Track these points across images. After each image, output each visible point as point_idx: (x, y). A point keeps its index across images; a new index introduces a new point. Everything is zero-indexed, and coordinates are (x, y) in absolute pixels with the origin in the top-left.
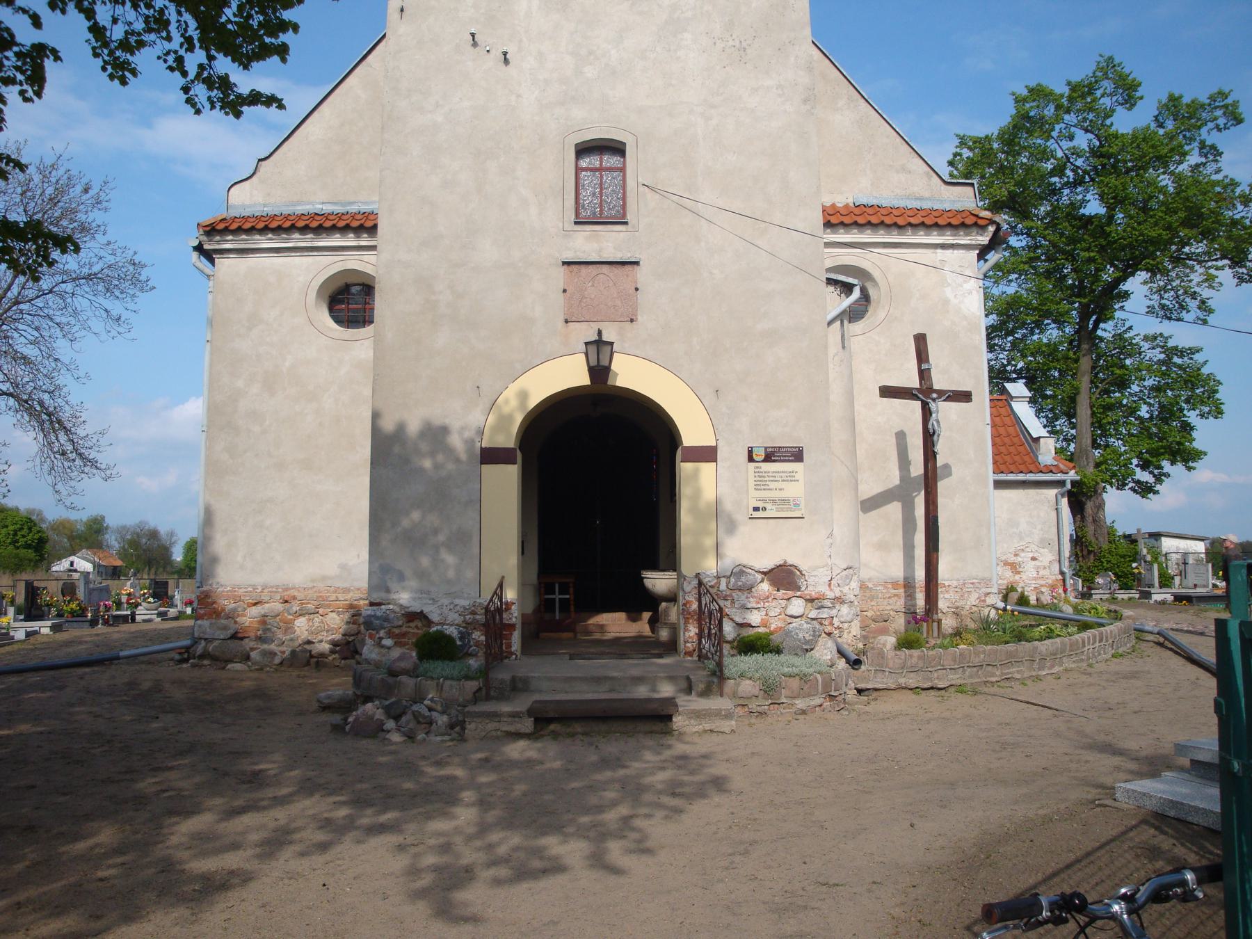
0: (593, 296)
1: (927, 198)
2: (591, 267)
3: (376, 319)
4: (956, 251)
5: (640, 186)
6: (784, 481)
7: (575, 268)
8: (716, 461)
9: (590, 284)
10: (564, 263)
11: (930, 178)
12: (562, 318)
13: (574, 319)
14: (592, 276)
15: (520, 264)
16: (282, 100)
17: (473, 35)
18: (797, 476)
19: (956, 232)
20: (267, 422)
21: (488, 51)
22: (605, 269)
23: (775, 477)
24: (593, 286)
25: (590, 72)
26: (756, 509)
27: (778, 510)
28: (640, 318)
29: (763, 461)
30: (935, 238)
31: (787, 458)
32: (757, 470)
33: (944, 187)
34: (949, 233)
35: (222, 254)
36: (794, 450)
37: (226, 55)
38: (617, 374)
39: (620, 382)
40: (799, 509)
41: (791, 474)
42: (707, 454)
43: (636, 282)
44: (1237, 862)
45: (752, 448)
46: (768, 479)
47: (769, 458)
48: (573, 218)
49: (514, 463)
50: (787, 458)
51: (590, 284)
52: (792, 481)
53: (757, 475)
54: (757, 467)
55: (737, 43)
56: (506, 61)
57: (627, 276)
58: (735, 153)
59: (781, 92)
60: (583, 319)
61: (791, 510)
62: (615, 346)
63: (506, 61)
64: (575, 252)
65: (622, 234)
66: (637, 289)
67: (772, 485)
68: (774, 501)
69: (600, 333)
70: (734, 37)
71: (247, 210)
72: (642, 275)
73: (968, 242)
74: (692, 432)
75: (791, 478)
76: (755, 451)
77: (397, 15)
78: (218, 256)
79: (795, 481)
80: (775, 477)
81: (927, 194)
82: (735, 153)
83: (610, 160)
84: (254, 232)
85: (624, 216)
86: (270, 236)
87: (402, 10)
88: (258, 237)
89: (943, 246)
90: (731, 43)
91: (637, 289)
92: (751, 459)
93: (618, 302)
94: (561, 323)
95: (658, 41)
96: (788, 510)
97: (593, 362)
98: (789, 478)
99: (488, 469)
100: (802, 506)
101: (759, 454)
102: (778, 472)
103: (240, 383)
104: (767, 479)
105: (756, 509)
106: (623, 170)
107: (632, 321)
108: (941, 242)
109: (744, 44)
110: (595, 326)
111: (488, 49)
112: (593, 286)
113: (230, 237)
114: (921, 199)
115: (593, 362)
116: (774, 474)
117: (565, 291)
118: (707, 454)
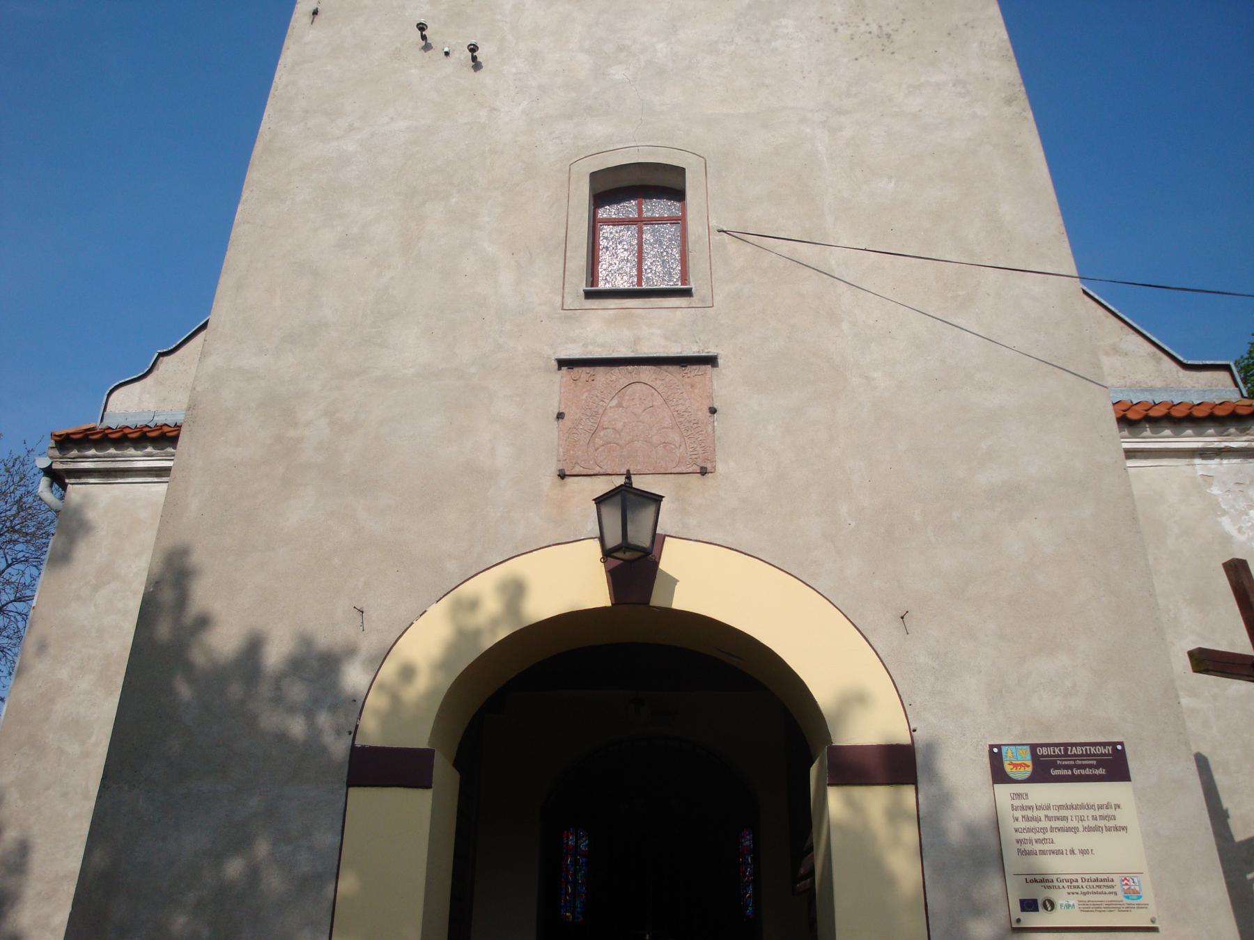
0: (619, 425)
1: (1160, 389)
2: (616, 370)
4: (1225, 461)
5: (714, 232)
6: (1089, 829)
7: (583, 372)
9: (614, 402)
10: (563, 363)
11: (1159, 361)
13: (577, 470)
14: (619, 387)
15: (473, 370)
17: (422, 27)
18: (1122, 818)
19: (1222, 429)
20: (93, 739)
21: (447, 54)
22: (646, 373)
23: (1064, 818)
24: (619, 405)
25: (618, 73)
27: (1086, 908)
28: (720, 467)
29: (1030, 780)
30: (1189, 440)
31: (1088, 772)
32: (1017, 803)
33: (1183, 374)
34: (1211, 431)
35: (79, 478)
36: (1102, 750)
38: (675, 581)
39: (683, 601)
40: (1140, 907)
41: (1104, 812)
43: (711, 397)
45: (999, 746)
46: (1047, 824)
48: (583, 287)
49: (425, 784)
50: (1088, 772)
51: (614, 402)
52: (1109, 829)
53: (1019, 814)
54: (1019, 796)
56: (477, 65)
57: (692, 386)
58: (890, 177)
59: (963, 90)
60: (597, 470)
62: (664, 504)
63: (477, 65)
64: (585, 345)
65: (679, 313)
66: (713, 411)
70: (867, 20)
71: (129, 419)
73: (1245, 444)
75: (1105, 821)
76: (1008, 754)
77: (306, 20)
78: (73, 481)
79: (1116, 829)
80: (1064, 818)
81: (1159, 384)
82: (890, 177)
83: (658, 208)
84: (127, 444)
85: (684, 277)
86: (150, 449)
87: (315, 13)
88: (132, 451)
89: (1204, 453)
90: (863, 28)
91: (713, 411)
93: (674, 437)
95: (738, 30)
96: (1111, 907)
98: (1101, 823)
99: (362, 798)
100: (1148, 895)
101: (1018, 761)
102: (1072, 807)
103: (64, 674)
104: (1044, 824)
106: (680, 221)
107: (704, 472)
108: (1200, 445)
109: (887, 30)
111: (446, 49)
112: (619, 405)
113: (92, 452)
114: (1151, 390)
116: (1063, 813)
117: (560, 416)
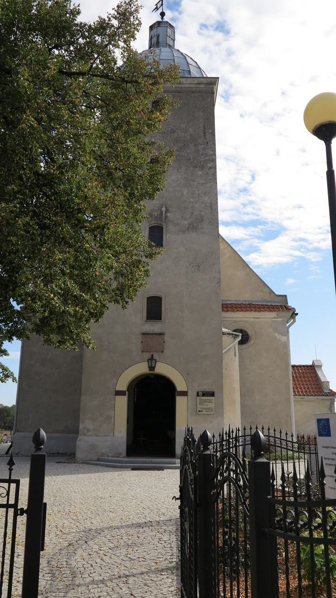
3: (146, 300)
7: (145, 335)
22: (155, 336)
28: (165, 351)
37: (2, 346)
42: (184, 394)
44: (198, 595)
47: (203, 395)
66: (164, 342)
67: (205, 404)
68: (205, 409)
69: (152, 356)
72: (166, 338)
74: (180, 386)
75: (210, 402)
81: (270, 299)
91: (164, 342)
92: (198, 395)
94: (140, 352)
97: (150, 365)
101: (201, 394)
107: (162, 352)
110: (151, 353)
114: (267, 302)
115: (150, 365)
117: (142, 342)
118: (184, 394)
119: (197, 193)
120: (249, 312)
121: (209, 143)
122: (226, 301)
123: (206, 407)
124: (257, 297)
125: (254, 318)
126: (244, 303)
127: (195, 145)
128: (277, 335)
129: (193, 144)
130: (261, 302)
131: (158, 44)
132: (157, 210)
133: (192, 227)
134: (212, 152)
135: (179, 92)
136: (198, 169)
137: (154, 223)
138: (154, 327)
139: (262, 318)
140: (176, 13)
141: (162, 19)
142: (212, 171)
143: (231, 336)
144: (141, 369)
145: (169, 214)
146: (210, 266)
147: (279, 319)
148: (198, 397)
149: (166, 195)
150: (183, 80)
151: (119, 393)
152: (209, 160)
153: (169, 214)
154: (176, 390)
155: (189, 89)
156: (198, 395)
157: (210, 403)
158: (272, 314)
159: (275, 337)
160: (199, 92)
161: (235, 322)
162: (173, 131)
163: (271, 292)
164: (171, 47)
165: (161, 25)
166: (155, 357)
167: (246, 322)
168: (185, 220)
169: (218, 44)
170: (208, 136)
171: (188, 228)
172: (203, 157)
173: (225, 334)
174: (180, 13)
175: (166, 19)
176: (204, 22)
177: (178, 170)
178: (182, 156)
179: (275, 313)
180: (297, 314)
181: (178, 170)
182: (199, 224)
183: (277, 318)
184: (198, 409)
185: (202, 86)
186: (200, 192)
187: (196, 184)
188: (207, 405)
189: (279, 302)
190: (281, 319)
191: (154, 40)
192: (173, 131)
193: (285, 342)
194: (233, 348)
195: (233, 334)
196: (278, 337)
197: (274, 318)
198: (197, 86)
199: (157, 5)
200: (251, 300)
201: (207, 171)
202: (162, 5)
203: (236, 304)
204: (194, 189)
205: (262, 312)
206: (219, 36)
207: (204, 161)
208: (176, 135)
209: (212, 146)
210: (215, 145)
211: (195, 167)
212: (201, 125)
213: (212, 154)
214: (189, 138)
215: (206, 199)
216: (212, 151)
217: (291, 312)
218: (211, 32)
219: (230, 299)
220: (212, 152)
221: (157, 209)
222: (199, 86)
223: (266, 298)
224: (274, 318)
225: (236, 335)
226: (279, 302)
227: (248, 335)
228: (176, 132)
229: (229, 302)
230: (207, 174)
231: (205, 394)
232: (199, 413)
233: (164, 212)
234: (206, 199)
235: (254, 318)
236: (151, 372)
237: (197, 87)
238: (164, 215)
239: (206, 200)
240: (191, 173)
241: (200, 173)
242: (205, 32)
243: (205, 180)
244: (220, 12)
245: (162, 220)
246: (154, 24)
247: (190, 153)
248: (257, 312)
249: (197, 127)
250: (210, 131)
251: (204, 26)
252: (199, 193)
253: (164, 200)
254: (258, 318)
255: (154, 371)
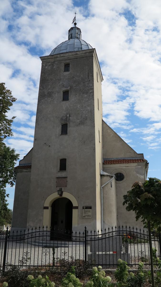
8: (44, 207)
12: (56, 186)
16: (15, 62)
18: (91, 211)
26: (84, 217)
27: (87, 217)
42: (77, 208)
55: (84, 141)
61: (89, 217)
67: (87, 213)
68: (87, 215)
72: (68, 179)
74: (75, 204)
75: (89, 211)
81: (134, 156)
92: (83, 209)
101: (84, 208)
105: (84, 217)
114: (133, 157)
117: (56, 182)
118: (77, 208)
119: (84, 106)
120: (122, 164)
121: (90, 81)
122: (111, 158)
123: (87, 214)
124: (128, 156)
125: (126, 167)
126: (121, 159)
127: (84, 83)
128: (138, 175)
129: (83, 82)
130: (130, 158)
131: (71, 38)
132: (65, 116)
133: (82, 123)
134: (92, 85)
135: (76, 59)
136: (85, 94)
137: (63, 122)
138: (63, 174)
139: (130, 166)
140: (134, 27)
141: (75, 26)
142: (92, 94)
143: (109, 177)
144: (55, 196)
145: (70, 118)
146: (90, 142)
147: (139, 167)
148: (83, 209)
149: (69, 108)
150: (78, 53)
151: (46, 208)
152: (90, 89)
153: (70, 118)
154: (73, 206)
155: (81, 57)
156: (83, 209)
157: (89, 212)
158: (135, 164)
159: (138, 176)
160: (86, 57)
161: (116, 169)
162: (73, 77)
163: (135, 152)
164: (78, 38)
165: (73, 29)
166: (63, 190)
167: (122, 169)
168: (78, 120)
169: (155, 37)
170: (90, 77)
171: (80, 123)
172: (87, 88)
173: (105, 176)
174: (136, 26)
175: (77, 26)
176: (147, 29)
177: (75, 95)
178: (77, 89)
179: (137, 163)
180: (148, 163)
181: (75, 95)
182: (85, 121)
183: (138, 166)
184: (83, 216)
185: (88, 54)
186: (86, 105)
187: (84, 101)
188: (88, 214)
189: (139, 158)
190: (140, 167)
191: (70, 36)
192: (73, 77)
193: (143, 178)
194: (110, 183)
195: (109, 176)
196: (139, 176)
197: (136, 166)
198: (85, 54)
199: (73, 20)
200: (125, 157)
201: (89, 94)
202: (75, 20)
203: (116, 160)
204: (83, 104)
205: (129, 163)
206: (155, 33)
207: (88, 90)
208: (74, 79)
209: (92, 82)
210: (93, 81)
211: (83, 93)
212: (87, 73)
213: (92, 86)
214: (81, 80)
215: (89, 108)
216: (92, 84)
217: (145, 163)
218: (151, 32)
219: (113, 158)
220: (92, 85)
221: (65, 116)
222: (86, 54)
223: (132, 156)
224: (136, 166)
225: (111, 176)
226: (139, 158)
227: (123, 176)
228: (75, 78)
229: (113, 159)
230: (89, 96)
231: (87, 208)
232: (84, 218)
233: (68, 117)
234: (89, 108)
235: (126, 167)
236: (61, 197)
237: (85, 55)
238: (68, 118)
239: (88, 108)
240: (82, 96)
241: (86, 96)
242: (147, 32)
243: (88, 99)
244: (155, 23)
245: (67, 121)
246: (70, 29)
247: (81, 87)
248: (127, 164)
249: (85, 73)
250: (91, 75)
251: (147, 30)
252: (85, 106)
253: (69, 111)
254: (128, 167)
255: (62, 196)
